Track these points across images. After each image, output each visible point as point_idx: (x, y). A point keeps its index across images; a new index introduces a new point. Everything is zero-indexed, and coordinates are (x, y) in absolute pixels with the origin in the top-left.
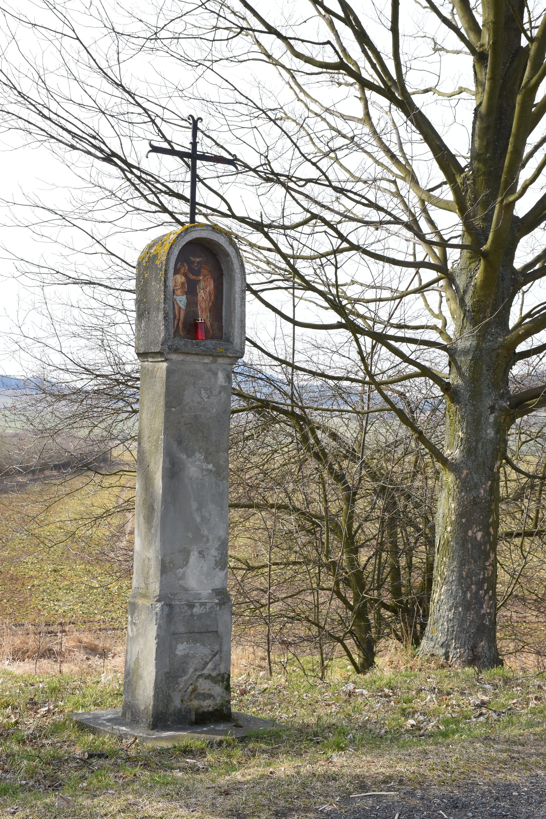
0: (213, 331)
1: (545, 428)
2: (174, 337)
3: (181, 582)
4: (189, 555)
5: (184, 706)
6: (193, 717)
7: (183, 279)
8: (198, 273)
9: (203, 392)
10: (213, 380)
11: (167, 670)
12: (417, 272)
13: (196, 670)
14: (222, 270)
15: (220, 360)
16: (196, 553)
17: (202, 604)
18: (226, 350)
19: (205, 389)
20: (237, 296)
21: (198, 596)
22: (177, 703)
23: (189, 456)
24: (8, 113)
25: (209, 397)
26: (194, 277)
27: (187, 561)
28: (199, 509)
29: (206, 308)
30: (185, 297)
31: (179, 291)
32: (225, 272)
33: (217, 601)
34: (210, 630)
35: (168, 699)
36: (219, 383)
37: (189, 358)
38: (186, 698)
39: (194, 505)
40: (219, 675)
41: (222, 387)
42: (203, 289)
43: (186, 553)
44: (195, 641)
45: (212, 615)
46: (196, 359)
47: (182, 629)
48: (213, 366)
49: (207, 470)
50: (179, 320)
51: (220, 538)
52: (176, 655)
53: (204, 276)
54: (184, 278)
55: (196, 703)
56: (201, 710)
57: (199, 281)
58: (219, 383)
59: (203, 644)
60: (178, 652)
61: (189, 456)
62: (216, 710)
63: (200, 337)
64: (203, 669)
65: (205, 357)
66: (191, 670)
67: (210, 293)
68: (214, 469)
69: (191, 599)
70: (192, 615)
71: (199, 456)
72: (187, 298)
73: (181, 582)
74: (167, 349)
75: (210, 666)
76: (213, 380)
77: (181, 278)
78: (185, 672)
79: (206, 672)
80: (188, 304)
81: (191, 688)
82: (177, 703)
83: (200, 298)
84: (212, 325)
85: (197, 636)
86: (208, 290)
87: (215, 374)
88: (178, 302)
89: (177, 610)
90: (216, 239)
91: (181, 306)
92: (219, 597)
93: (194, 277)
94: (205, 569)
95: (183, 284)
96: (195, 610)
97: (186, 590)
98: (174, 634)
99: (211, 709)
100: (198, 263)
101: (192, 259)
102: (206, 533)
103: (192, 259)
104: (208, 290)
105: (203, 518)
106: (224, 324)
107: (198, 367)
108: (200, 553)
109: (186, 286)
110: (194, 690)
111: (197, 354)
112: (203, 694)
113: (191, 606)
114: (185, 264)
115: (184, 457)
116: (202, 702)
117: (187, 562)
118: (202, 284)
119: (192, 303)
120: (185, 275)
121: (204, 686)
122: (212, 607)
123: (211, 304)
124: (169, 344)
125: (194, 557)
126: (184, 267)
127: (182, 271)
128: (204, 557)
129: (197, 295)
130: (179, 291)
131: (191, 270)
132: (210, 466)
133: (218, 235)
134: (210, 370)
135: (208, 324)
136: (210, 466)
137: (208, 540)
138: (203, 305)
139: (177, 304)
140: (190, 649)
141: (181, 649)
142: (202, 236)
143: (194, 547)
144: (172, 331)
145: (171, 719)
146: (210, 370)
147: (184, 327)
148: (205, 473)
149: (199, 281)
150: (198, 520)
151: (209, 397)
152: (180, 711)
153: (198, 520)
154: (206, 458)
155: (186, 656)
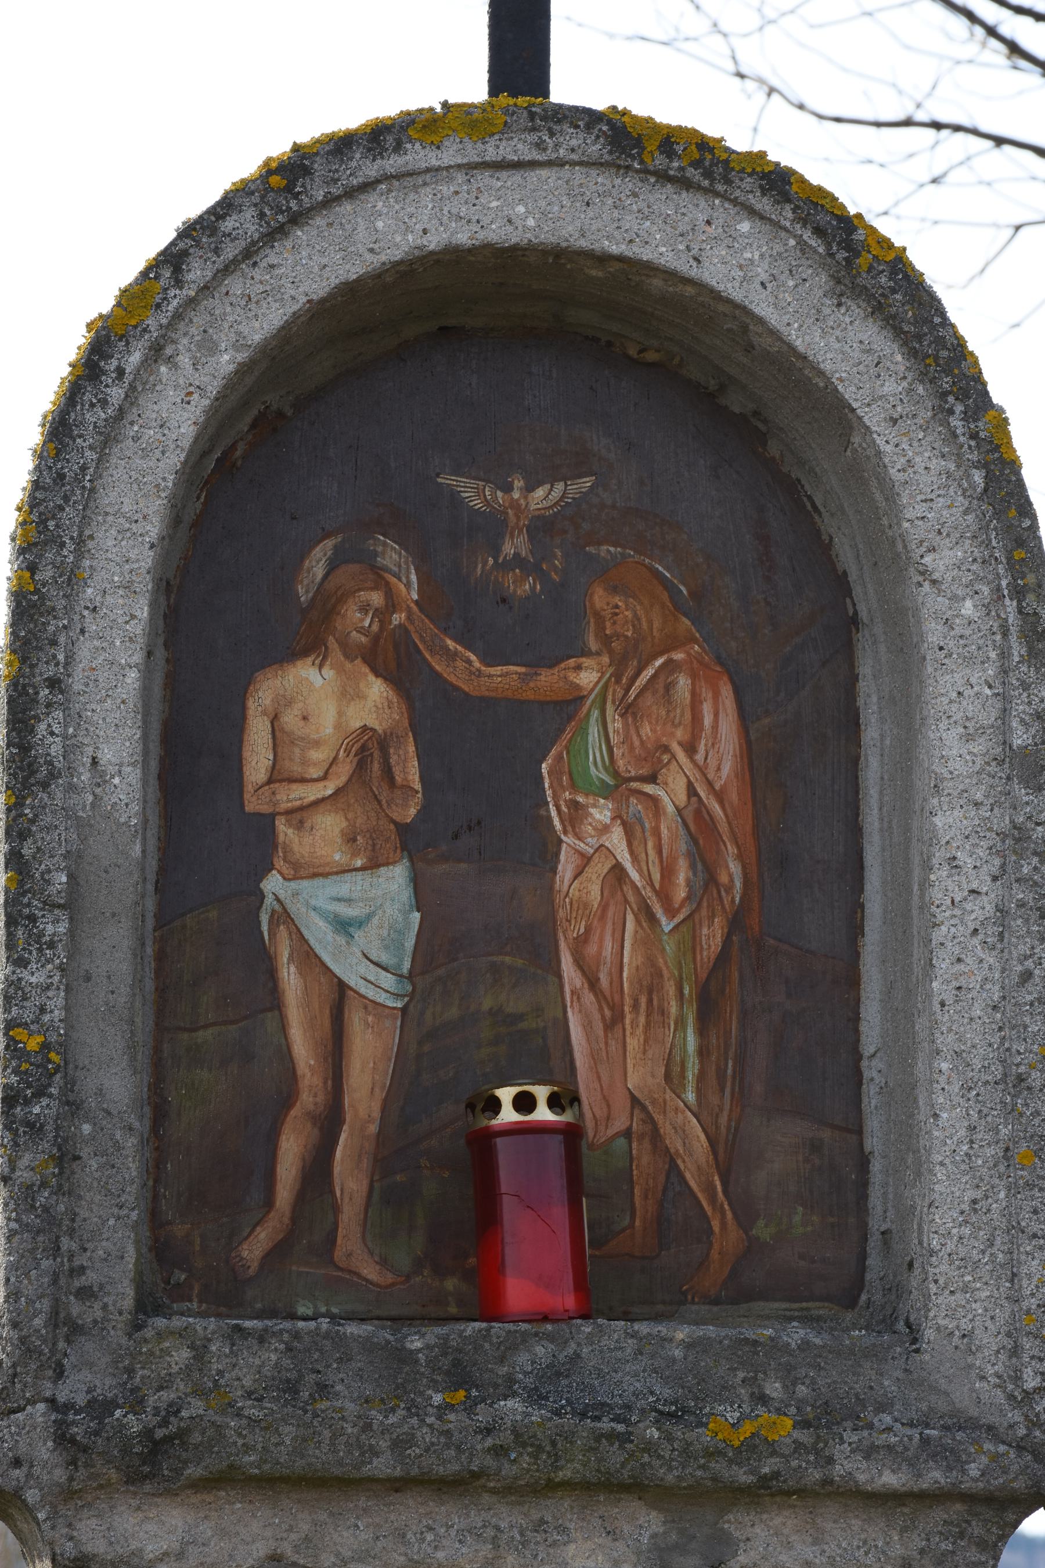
0: (746, 1214)
2: (147, 1306)
7: (375, 701)
8: (547, 632)
14: (842, 584)
18: (824, 1418)
20: (949, 821)
24: (937, 126)
26: (502, 677)
29: (651, 985)
30: (394, 880)
31: (330, 825)
32: (865, 600)
42: (617, 788)
50: (330, 1121)
53: (625, 660)
54: (376, 689)
57: (568, 707)
63: (517, 1292)
65: (560, 1509)
67: (699, 825)
72: (422, 893)
74: (44, 1451)
77: (348, 694)
80: (439, 955)
83: (576, 883)
84: (729, 1156)
86: (671, 793)
88: (320, 935)
90: (660, 250)
91: (353, 971)
93: (502, 677)
95: (369, 751)
100: (543, 527)
101: (473, 493)
103: (473, 493)
104: (671, 793)
106: (873, 1142)
109: (411, 772)
114: (391, 555)
119: (485, 941)
120: (393, 659)
123: (712, 936)
124: (73, 1389)
126: (378, 578)
127: (357, 619)
129: (547, 854)
130: (330, 825)
131: (456, 603)
133: (695, 209)
135: (691, 1141)
138: (624, 950)
139: (307, 957)
142: (497, 233)
144: (114, 1252)
147: (390, 1197)
149: (568, 707)
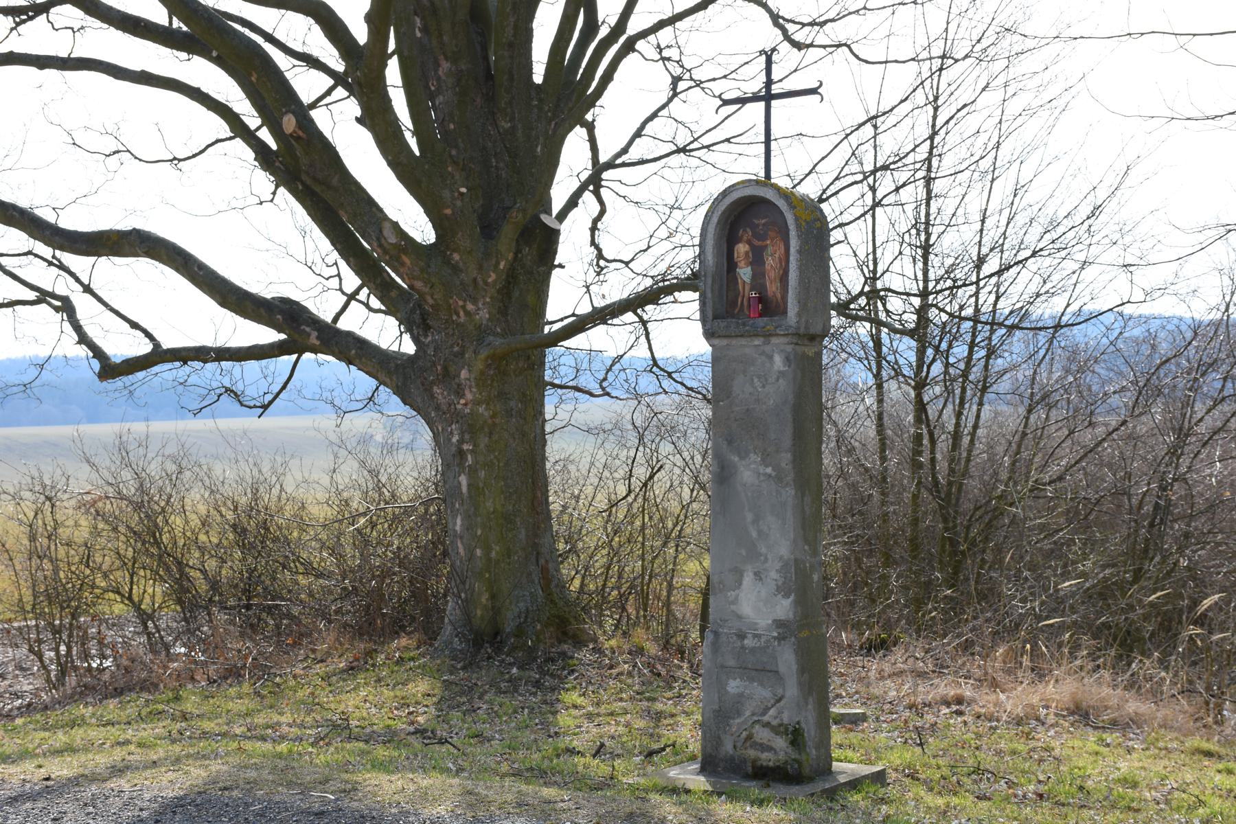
1: (1233, 420)
3: (733, 607)
4: (742, 576)
5: (738, 753)
6: (750, 769)
7: (747, 247)
8: (762, 238)
9: (756, 380)
10: (768, 365)
11: (716, 707)
12: (821, 200)
13: (753, 714)
15: (774, 340)
16: (751, 574)
17: (755, 636)
19: (759, 377)
21: (754, 626)
22: (728, 747)
23: (741, 458)
25: (764, 386)
27: (739, 583)
28: (756, 521)
33: (775, 634)
34: (768, 668)
35: (718, 742)
36: (776, 368)
37: (734, 341)
38: (739, 745)
39: (749, 517)
40: (780, 725)
41: (780, 372)
43: (739, 574)
44: (752, 680)
45: (770, 651)
46: (743, 341)
47: (731, 662)
48: (767, 349)
49: (765, 474)
51: (781, 558)
52: (727, 692)
55: (752, 753)
56: (759, 763)
58: (776, 368)
59: (762, 684)
60: (729, 689)
61: (741, 458)
62: (778, 767)
64: (764, 714)
66: (748, 713)
68: (774, 474)
69: (744, 629)
70: (743, 647)
71: (754, 458)
73: (733, 607)
75: (772, 712)
76: (768, 365)
78: (739, 713)
79: (766, 718)
81: (744, 734)
82: (728, 747)
83: (767, 267)
85: (754, 673)
87: (771, 358)
89: (723, 639)
92: (780, 630)
94: (763, 593)
95: (747, 253)
96: (746, 642)
97: (740, 617)
98: (723, 667)
99: (771, 764)
101: (756, 222)
102: (764, 550)
105: (760, 532)
107: (747, 350)
108: (755, 574)
110: (750, 737)
111: (742, 336)
112: (761, 745)
113: (742, 636)
115: (736, 459)
116: (759, 753)
117: (740, 584)
118: (770, 250)
120: (749, 242)
121: (762, 735)
122: (768, 641)
125: (748, 579)
128: (761, 579)
132: (769, 470)
134: (763, 353)
136: (769, 470)
137: (766, 560)
138: (772, 274)
140: (746, 687)
141: (734, 686)
143: (749, 567)
145: (721, 765)
146: (763, 353)
148: (762, 478)
149: (766, 246)
150: (754, 534)
151: (764, 386)
152: (732, 759)
153: (754, 534)
154: (763, 460)
155: (741, 695)
